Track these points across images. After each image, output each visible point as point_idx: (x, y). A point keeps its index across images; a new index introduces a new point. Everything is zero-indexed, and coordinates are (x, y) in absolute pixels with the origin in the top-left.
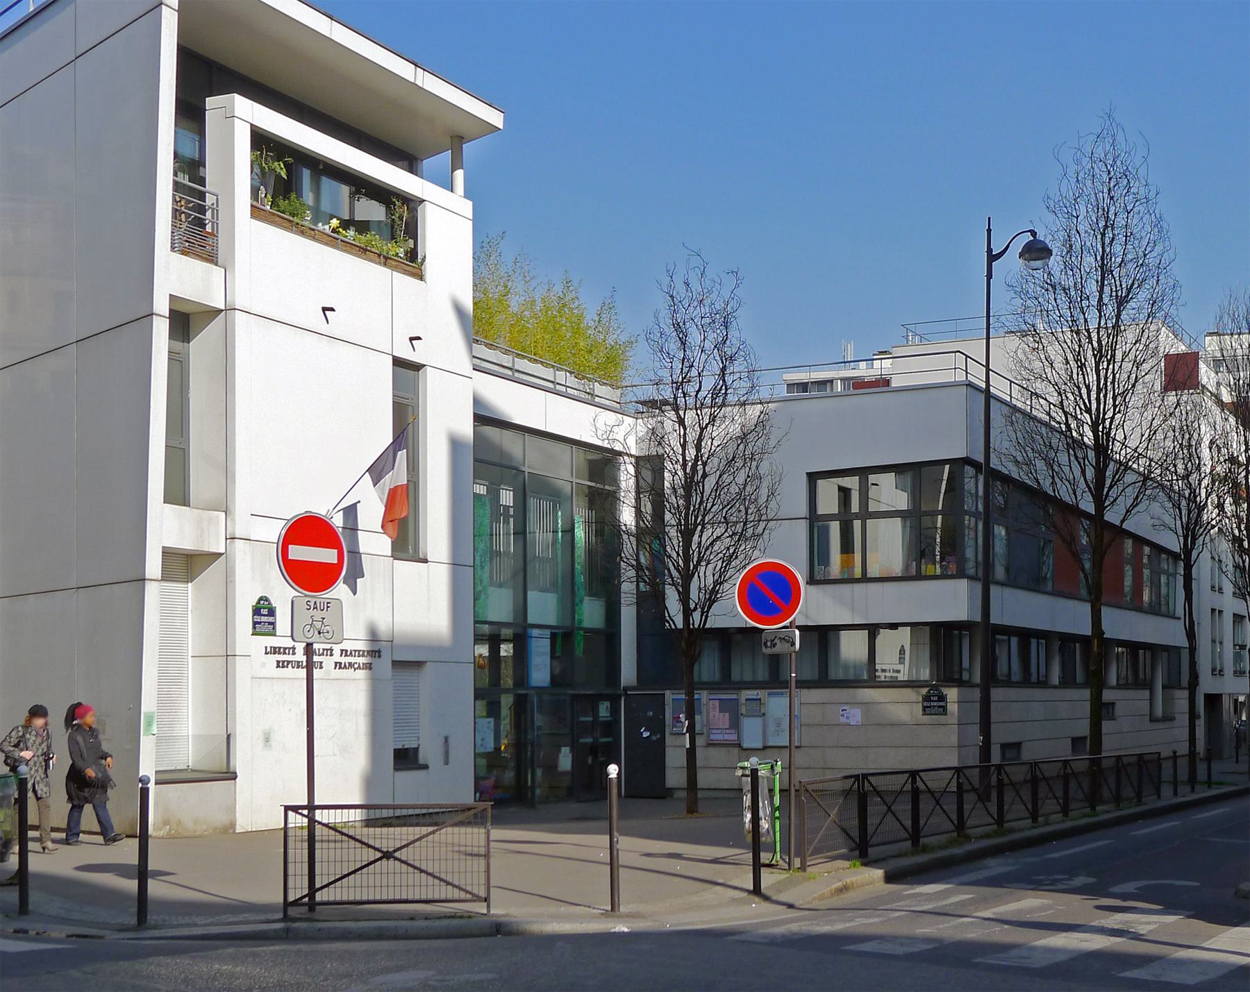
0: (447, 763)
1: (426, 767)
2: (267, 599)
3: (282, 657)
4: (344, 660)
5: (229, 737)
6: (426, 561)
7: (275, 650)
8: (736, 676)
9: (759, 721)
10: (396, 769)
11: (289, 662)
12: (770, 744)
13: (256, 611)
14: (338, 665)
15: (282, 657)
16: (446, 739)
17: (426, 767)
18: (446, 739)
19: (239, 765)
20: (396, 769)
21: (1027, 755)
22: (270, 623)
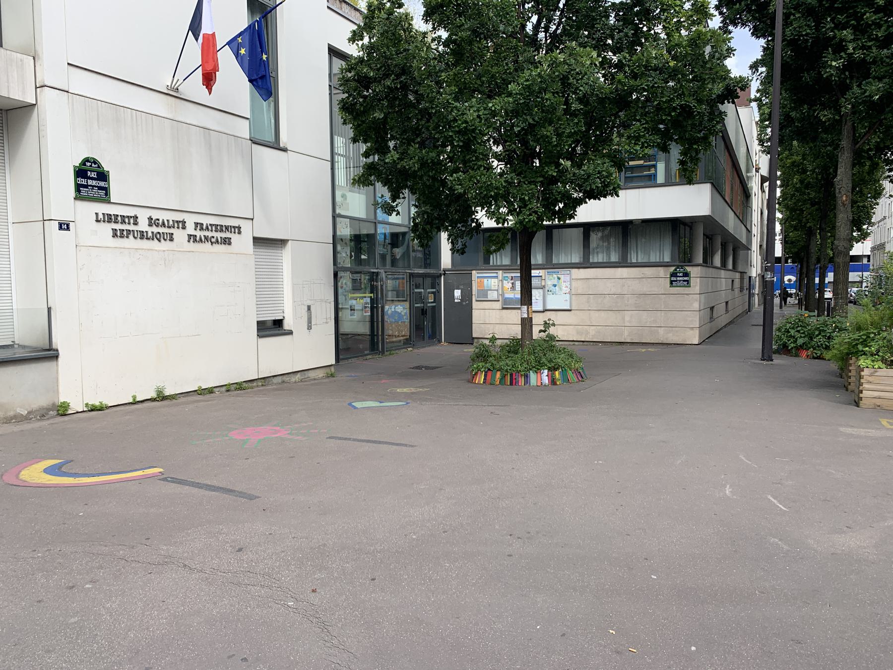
0: (309, 328)
1: (290, 333)
2: (95, 162)
3: (118, 227)
4: (199, 233)
5: (49, 309)
6: (285, 150)
7: (109, 218)
8: (555, 261)
9: (345, 328)
10: (259, 336)
11: (129, 231)
12: (548, 308)
13: (80, 173)
14: (192, 238)
15: (118, 227)
16: (309, 308)
17: (290, 333)
18: (309, 308)
19: (58, 342)
20: (259, 336)
21: (552, 331)
22: (100, 188)
